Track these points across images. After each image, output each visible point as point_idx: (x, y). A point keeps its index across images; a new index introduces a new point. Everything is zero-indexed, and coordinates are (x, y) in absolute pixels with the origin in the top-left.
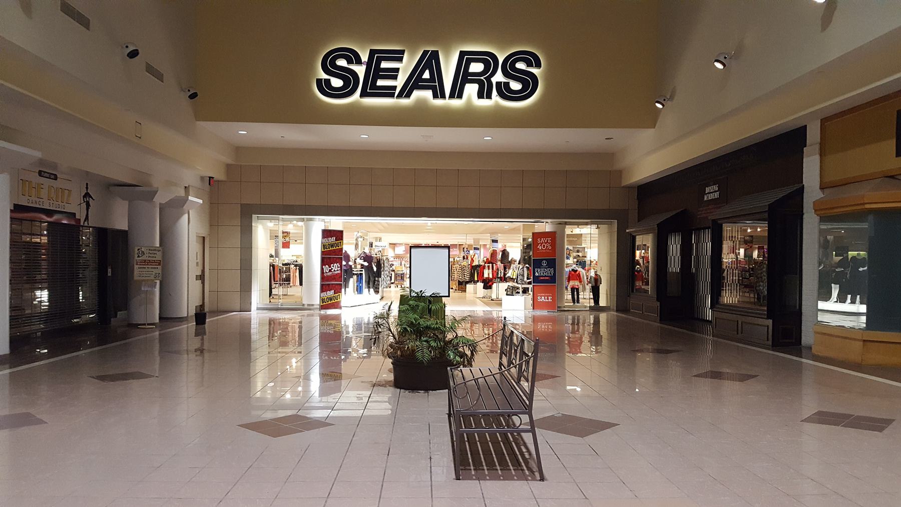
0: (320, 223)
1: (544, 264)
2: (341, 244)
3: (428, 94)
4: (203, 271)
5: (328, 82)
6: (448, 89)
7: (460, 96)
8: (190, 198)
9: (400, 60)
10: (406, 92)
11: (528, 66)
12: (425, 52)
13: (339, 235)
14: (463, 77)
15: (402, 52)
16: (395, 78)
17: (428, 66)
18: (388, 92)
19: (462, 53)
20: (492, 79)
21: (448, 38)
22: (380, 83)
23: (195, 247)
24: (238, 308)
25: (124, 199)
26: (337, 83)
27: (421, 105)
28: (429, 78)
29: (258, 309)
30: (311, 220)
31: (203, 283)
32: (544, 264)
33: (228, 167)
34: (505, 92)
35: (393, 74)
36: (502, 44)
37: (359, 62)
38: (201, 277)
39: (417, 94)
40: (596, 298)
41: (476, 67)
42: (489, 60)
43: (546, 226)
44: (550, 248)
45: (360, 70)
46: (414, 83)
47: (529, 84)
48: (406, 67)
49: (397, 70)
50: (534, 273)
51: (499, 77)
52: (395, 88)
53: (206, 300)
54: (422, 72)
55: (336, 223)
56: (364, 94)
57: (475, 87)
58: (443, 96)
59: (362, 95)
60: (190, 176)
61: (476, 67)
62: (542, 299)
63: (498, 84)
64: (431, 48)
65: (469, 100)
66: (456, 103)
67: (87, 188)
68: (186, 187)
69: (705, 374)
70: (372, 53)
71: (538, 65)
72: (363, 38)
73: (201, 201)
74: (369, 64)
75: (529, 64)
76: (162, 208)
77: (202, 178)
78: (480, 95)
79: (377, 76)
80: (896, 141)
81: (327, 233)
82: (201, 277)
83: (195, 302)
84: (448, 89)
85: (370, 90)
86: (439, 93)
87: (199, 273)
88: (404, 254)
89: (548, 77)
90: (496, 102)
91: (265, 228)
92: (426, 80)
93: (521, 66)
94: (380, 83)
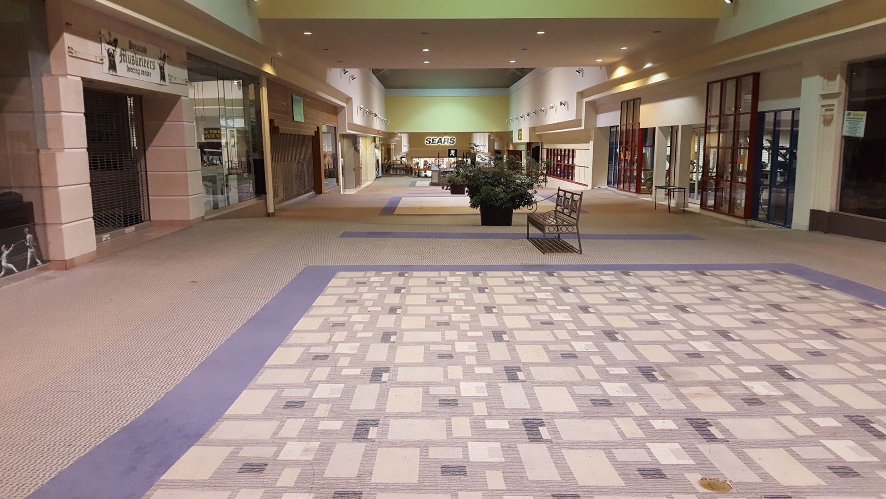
14: (445, 141)
18: (435, 143)
20: (804, 81)
21: (443, 137)
28: (758, 111)
36: (450, 136)
45: (431, 141)
46: (438, 142)
48: (437, 140)
55: (425, 159)
69: (570, 472)
80: (248, 37)
81: (425, 161)
86: (441, 143)
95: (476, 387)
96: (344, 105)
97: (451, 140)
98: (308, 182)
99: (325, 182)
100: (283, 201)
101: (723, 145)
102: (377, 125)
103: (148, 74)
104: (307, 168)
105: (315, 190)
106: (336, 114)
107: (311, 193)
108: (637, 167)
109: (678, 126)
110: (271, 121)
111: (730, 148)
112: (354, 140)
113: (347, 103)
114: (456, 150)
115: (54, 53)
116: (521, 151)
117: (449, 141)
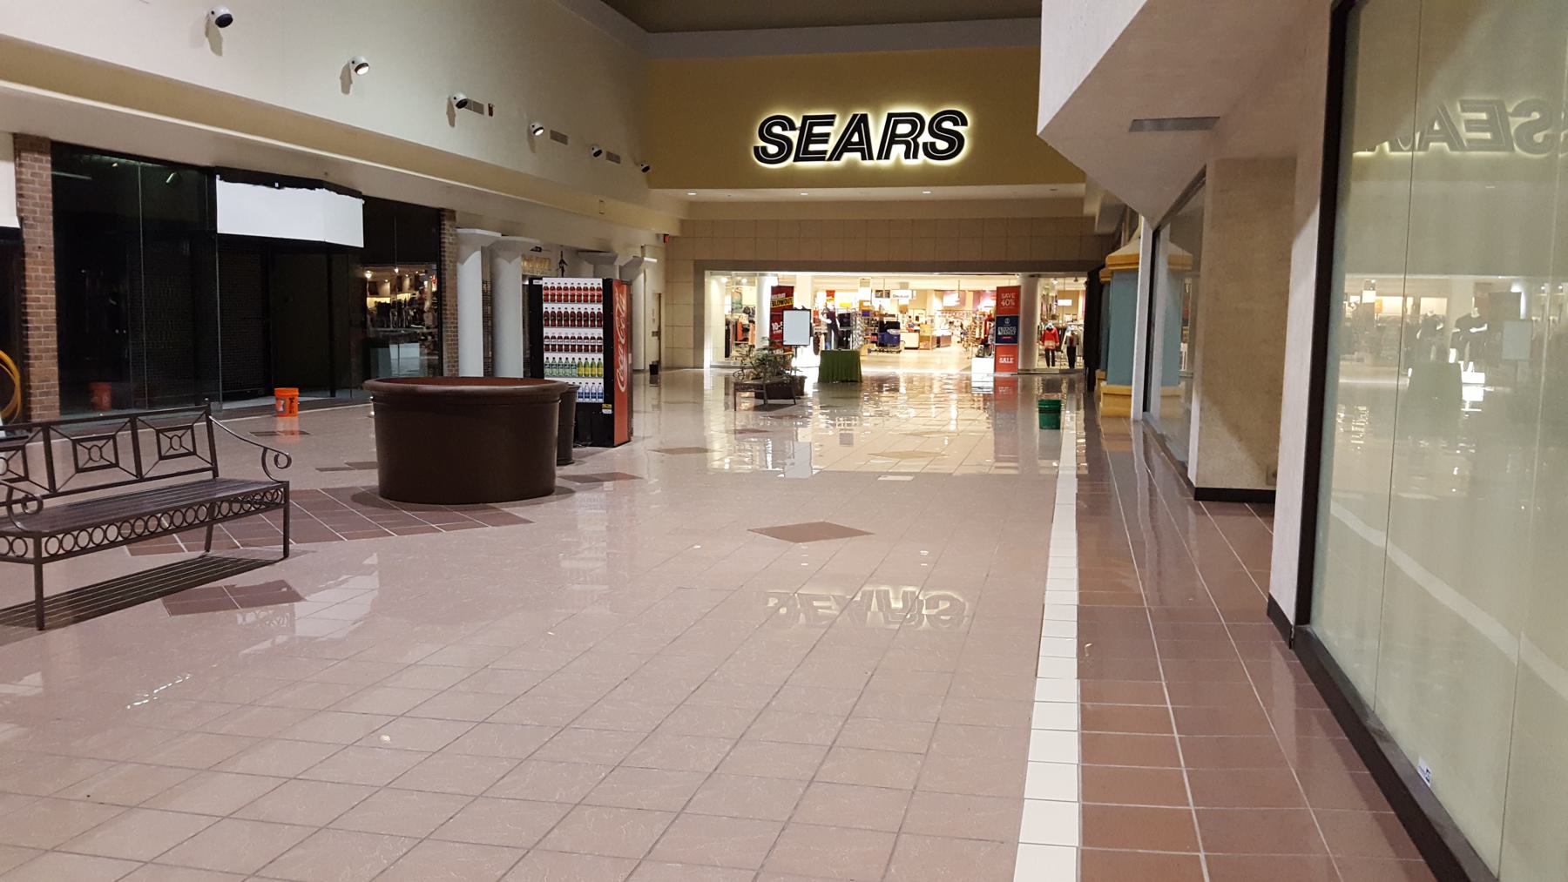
0: (772, 279)
1: (1007, 321)
2: (791, 300)
3: (858, 155)
4: (659, 327)
5: (764, 149)
6: (875, 151)
7: (887, 157)
8: (646, 259)
9: (831, 124)
10: (837, 154)
11: (954, 125)
12: (855, 116)
13: (789, 291)
14: (890, 139)
15: (833, 117)
16: (826, 142)
17: (857, 129)
18: (820, 156)
19: (890, 116)
21: (876, 103)
22: (812, 147)
23: (651, 304)
24: (692, 365)
25: (590, 263)
26: (773, 149)
27: (851, 166)
29: (711, 367)
30: (763, 275)
31: (659, 339)
32: (1007, 321)
33: (683, 223)
34: (931, 151)
35: (824, 138)
36: (929, 102)
37: (793, 128)
38: (658, 334)
39: (846, 156)
40: (1072, 362)
41: (904, 129)
42: (915, 120)
43: (1013, 280)
44: (1013, 304)
45: (793, 136)
46: (844, 146)
47: (956, 142)
48: (835, 131)
49: (828, 135)
50: (997, 332)
51: (926, 137)
52: (825, 152)
53: (663, 356)
54: (852, 135)
56: (796, 159)
57: (903, 148)
58: (871, 158)
59: (796, 159)
60: (646, 236)
61: (904, 129)
62: (1003, 361)
63: (925, 144)
64: (860, 112)
65: (898, 159)
66: (884, 163)
67: (562, 256)
68: (642, 247)
70: (805, 119)
71: (964, 123)
72: (796, 105)
73: (655, 260)
74: (802, 129)
75: (956, 124)
76: (621, 268)
77: (658, 235)
78: (907, 156)
79: (809, 142)
82: (658, 334)
83: (652, 359)
84: (875, 151)
85: (804, 154)
87: (656, 330)
88: (957, 306)
89: (977, 135)
90: (925, 161)
91: (719, 283)
92: (855, 144)
93: (947, 125)
94: (812, 147)
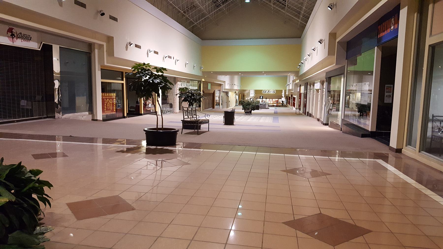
45: (265, 91)
46: (268, 92)
95: (60, 47)
96: (223, 83)
97: (273, 91)
98: (211, 105)
99: (216, 107)
100: (204, 109)
101: (241, 213)
102: (236, 87)
103: (185, 85)
104: (211, 102)
105: (212, 107)
106: (221, 86)
107: (211, 108)
108: (54, 84)
109: (102, 82)
110: (203, 90)
111: (363, 236)
112: (227, 93)
113: (224, 83)
114: (263, 97)
115: (176, 84)
116: (295, 98)
117: (273, 92)
